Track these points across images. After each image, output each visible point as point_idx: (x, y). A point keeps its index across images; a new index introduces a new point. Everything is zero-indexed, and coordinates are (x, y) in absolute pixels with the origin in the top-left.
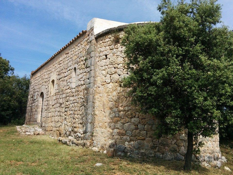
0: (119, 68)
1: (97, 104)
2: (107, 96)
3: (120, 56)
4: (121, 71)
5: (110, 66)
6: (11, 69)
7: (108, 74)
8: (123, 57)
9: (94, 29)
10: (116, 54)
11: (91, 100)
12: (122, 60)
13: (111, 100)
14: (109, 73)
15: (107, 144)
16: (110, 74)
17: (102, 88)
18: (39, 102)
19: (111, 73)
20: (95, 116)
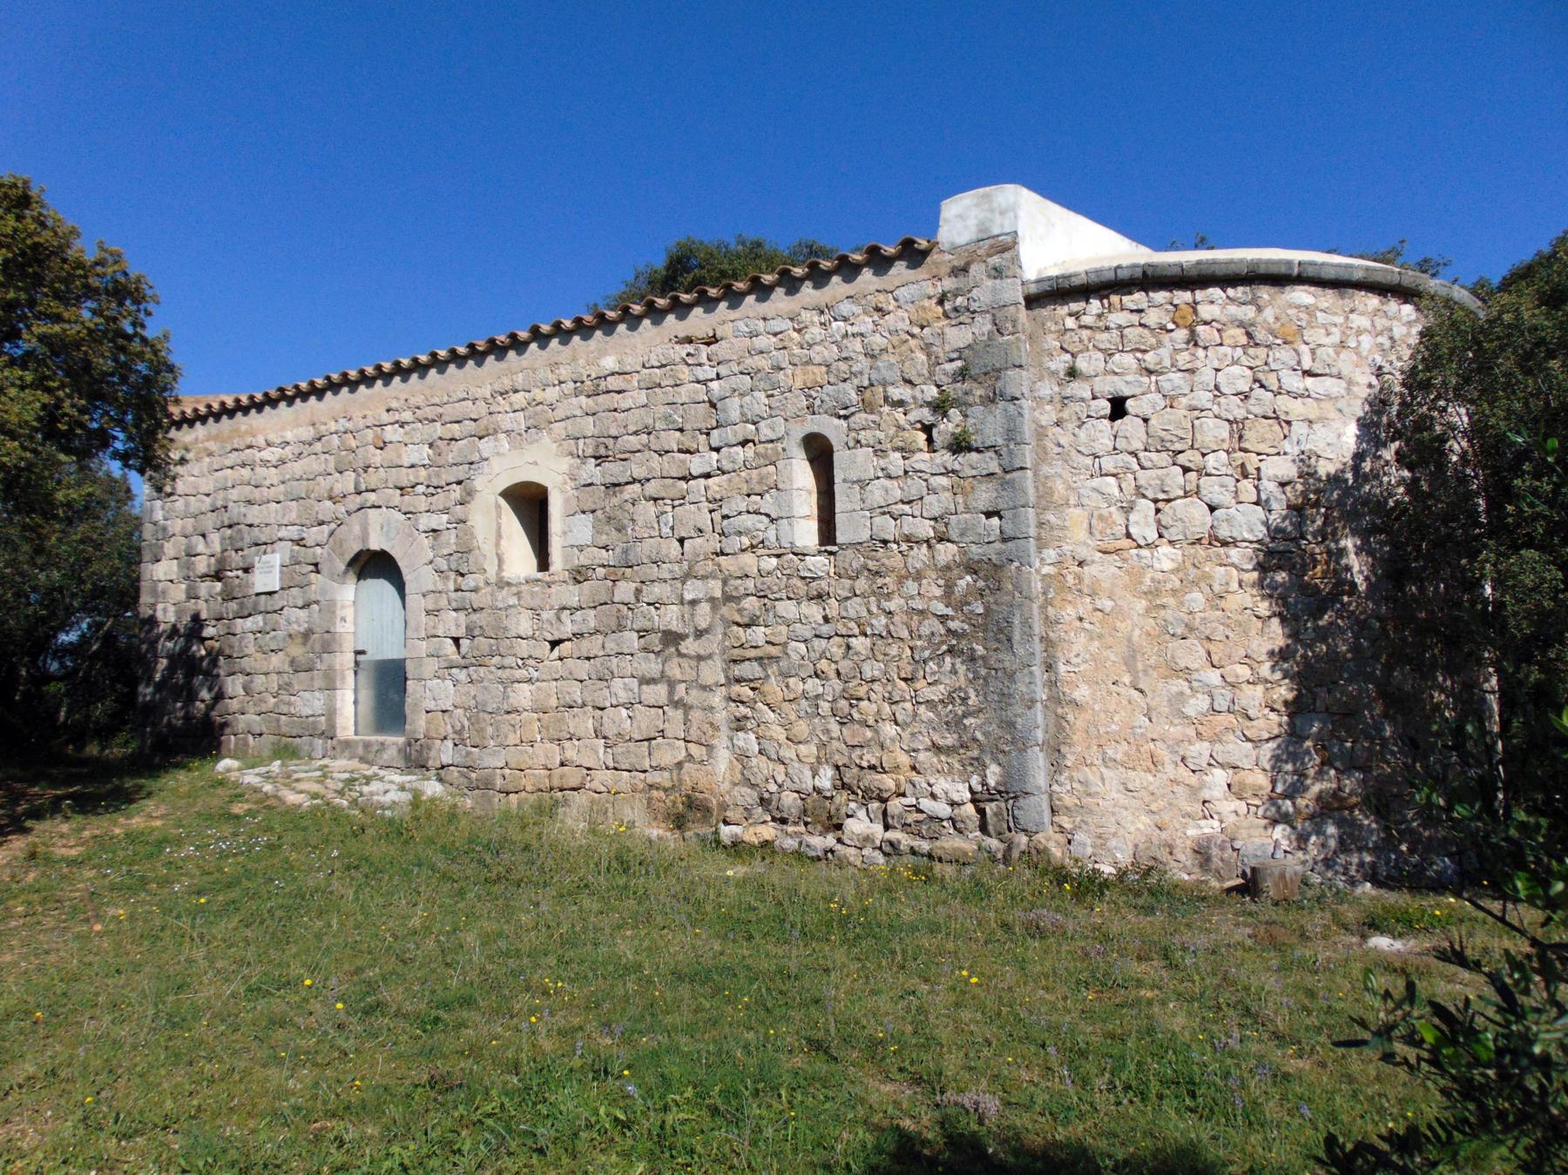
0: (1214, 472)
1: (1077, 651)
2: (1148, 611)
3: (1210, 414)
4: (1222, 486)
5: (1154, 456)
6: (71, 232)
7: (1144, 496)
8: (1228, 420)
9: (132, 487)
10: (1184, 400)
11: (1038, 628)
12: (1226, 435)
13: (1179, 631)
14: (1150, 494)
15: (1178, 842)
16: (1155, 501)
17: (1103, 570)
18: (339, 613)
19: (1162, 496)
20: (1060, 711)
